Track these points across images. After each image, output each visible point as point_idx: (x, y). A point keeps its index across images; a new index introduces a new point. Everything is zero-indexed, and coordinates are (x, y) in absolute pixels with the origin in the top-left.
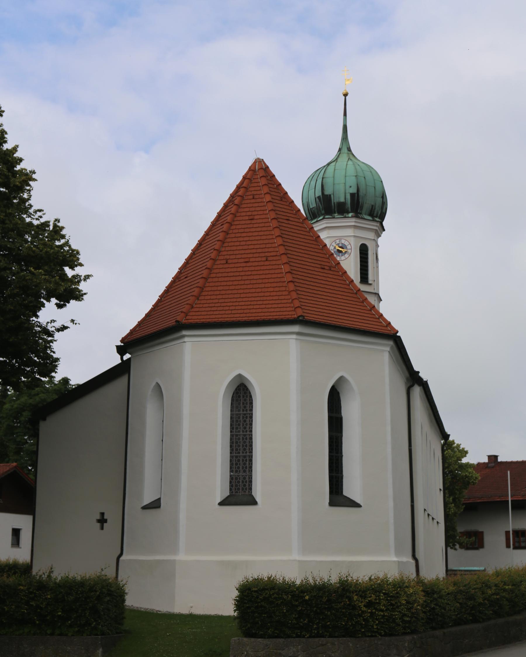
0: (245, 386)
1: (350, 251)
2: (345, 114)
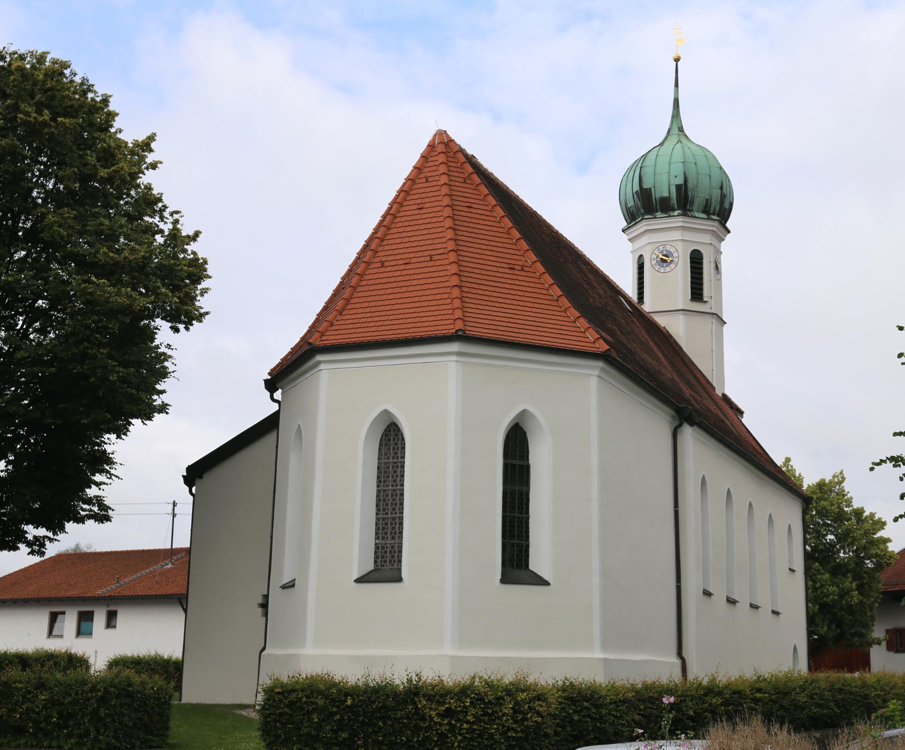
0: (397, 426)
1: (676, 260)
2: (677, 85)
